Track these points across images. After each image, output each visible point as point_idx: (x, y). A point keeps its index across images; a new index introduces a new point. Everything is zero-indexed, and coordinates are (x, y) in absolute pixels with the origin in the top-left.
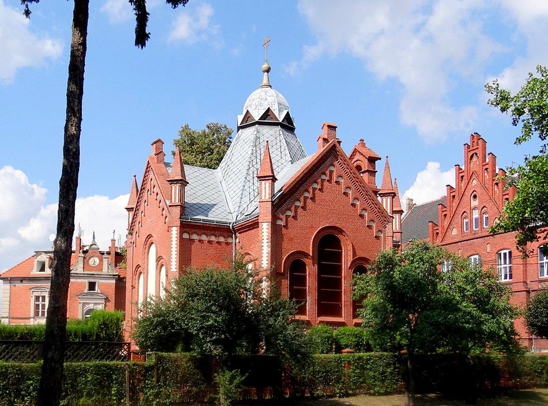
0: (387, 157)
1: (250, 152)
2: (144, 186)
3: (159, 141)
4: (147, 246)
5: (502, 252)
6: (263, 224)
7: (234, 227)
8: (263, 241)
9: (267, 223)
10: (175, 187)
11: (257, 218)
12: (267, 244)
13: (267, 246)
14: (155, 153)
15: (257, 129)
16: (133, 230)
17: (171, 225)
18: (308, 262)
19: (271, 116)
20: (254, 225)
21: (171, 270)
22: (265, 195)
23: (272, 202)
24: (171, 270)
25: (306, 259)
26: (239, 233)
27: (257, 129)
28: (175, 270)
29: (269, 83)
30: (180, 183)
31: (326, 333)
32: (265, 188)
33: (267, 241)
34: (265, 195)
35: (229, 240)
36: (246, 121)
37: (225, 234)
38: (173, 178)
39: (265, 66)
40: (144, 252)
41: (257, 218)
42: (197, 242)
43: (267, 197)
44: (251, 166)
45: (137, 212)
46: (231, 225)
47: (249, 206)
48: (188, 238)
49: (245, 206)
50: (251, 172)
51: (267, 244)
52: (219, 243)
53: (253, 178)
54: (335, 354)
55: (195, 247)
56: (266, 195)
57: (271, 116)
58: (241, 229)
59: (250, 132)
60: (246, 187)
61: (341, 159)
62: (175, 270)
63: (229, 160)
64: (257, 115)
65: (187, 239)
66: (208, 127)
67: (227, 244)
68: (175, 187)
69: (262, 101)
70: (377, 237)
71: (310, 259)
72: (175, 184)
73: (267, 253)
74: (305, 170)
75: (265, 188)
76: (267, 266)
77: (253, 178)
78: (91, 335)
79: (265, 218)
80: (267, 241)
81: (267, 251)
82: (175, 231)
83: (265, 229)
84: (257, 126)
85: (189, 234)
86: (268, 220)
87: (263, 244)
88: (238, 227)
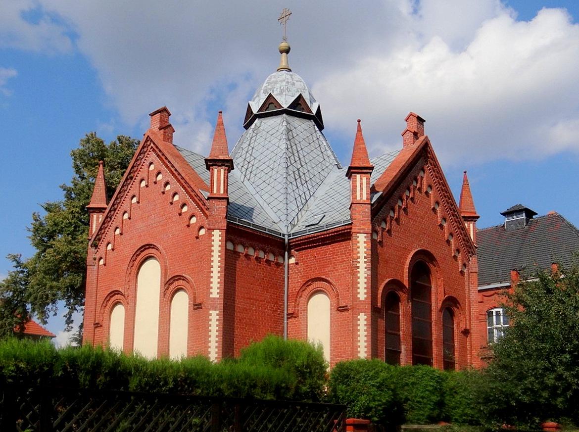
0: (465, 172)
1: (284, 146)
2: (132, 175)
3: (164, 110)
4: (136, 263)
5: (494, 311)
6: (358, 235)
7: (290, 241)
8: (358, 260)
9: (365, 235)
10: (219, 172)
11: (350, 227)
12: (365, 265)
13: (366, 268)
14: (159, 125)
15: (286, 119)
16: (99, 240)
17: (212, 227)
18: (403, 296)
19: (303, 106)
20: (343, 235)
21: (211, 296)
22: (361, 194)
23: (372, 205)
24: (211, 296)
25: (401, 293)
26: (297, 251)
27: (286, 119)
28: (218, 296)
29: (288, 66)
30: (227, 166)
31: (374, 401)
32: (361, 184)
33: (366, 260)
34: (361, 194)
35: (280, 260)
36: (266, 109)
37: (276, 250)
38: (216, 156)
39: (284, 45)
40: (129, 272)
41: (350, 227)
42: (242, 257)
43: (364, 198)
44: (289, 164)
45: (112, 212)
46: (286, 238)
47: (300, 216)
48: (232, 249)
49: (294, 214)
50: (291, 172)
51: (365, 265)
52: (268, 261)
53: (296, 180)
54: (492, 429)
55: (241, 263)
56: (363, 194)
57: (303, 106)
58: (304, 244)
59: (277, 123)
60: (290, 191)
61: (431, 164)
62: (218, 296)
63: (248, 155)
64: (285, 102)
65: (231, 251)
66: (119, 139)
67: (278, 265)
68: (219, 172)
69: (290, 86)
70: (462, 272)
71: (404, 293)
72: (218, 166)
73: (365, 278)
74: (402, 168)
75: (361, 184)
76: (366, 296)
77: (296, 180)
78: (287, 389)
79: (362, 227)
80: (366, 260)
81: (366, 275)
82: (217, 237)
83: (362, 243)
84: (284, 115)
85: (234, 244)
86: (366, 230)
87: (358, 265)
88: (303, 240)
